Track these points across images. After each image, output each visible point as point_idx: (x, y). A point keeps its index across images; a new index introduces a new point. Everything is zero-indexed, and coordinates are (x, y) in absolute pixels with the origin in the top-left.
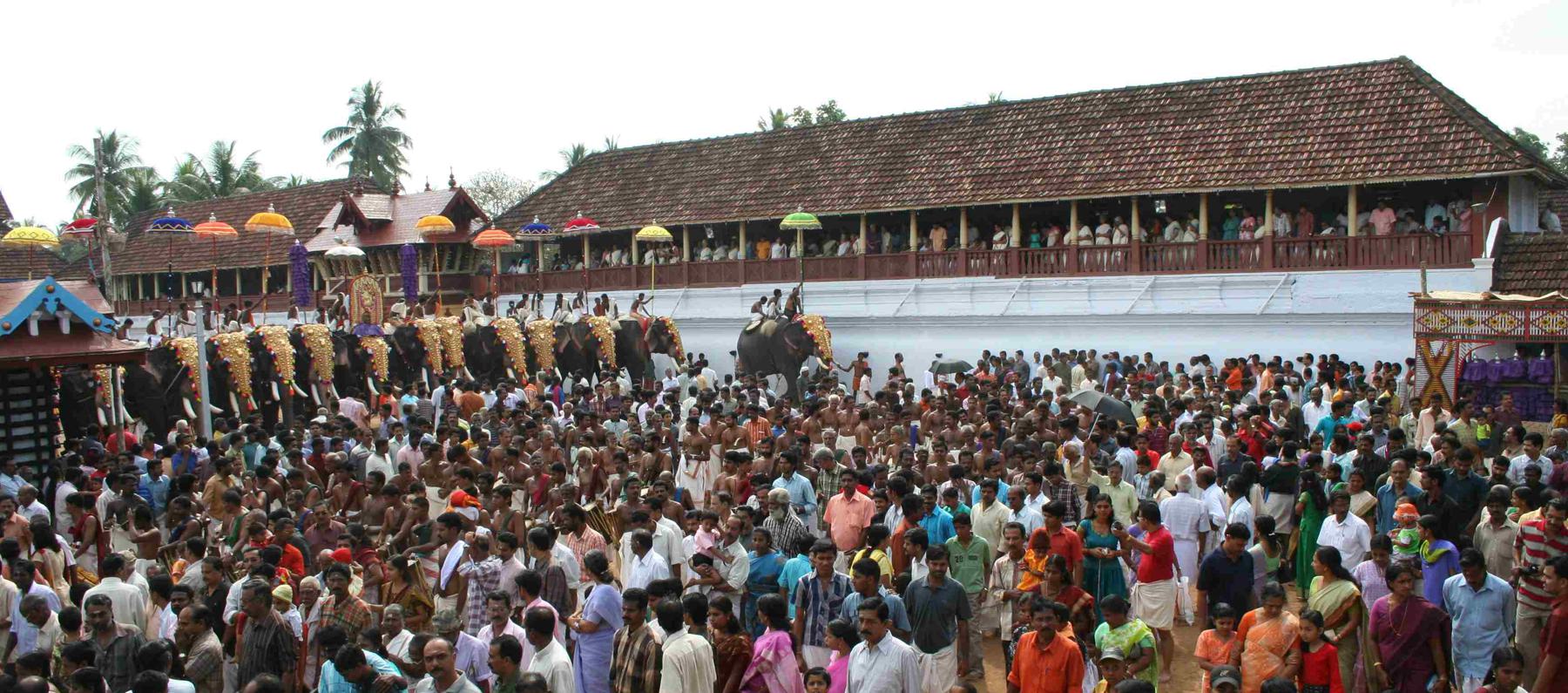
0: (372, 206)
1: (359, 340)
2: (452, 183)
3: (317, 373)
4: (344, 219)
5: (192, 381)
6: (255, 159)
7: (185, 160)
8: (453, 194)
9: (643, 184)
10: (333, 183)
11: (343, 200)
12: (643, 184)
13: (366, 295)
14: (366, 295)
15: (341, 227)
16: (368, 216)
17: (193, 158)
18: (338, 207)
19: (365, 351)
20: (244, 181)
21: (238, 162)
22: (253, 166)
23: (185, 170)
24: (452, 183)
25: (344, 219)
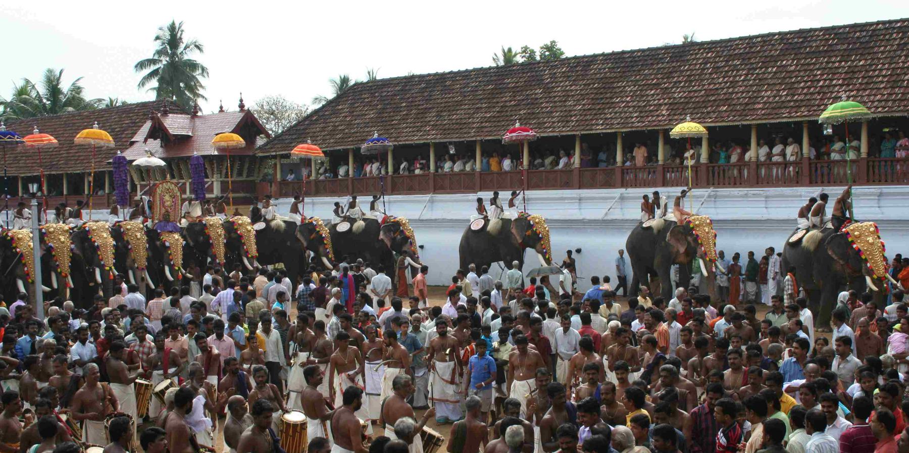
0: (175, 124)
1: (159, 235)
2: (242, 106)
3: (134, 261)
4: (152, 135)
5: (25, 265)
6: (79, 84)
7: (20, 84)
8: (242, 115)
9: (397, 110)
10: (144, 105)
11: (152, 119)
12: (397, 110)
13: (167, 198)
14: (167, 198)
15: (150, 141)
16: (171, 131)
17: (27, 81)
18: (148, 125)
19: (163, 244)
20: (69, 103)
21: (65, 86)
22: (77, 90)
23: (21, 92)
24: (242, 106)
25: (152, 135)
